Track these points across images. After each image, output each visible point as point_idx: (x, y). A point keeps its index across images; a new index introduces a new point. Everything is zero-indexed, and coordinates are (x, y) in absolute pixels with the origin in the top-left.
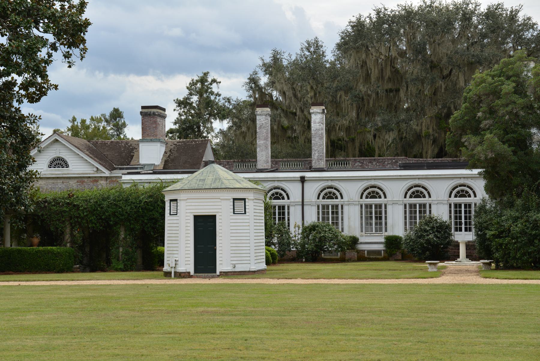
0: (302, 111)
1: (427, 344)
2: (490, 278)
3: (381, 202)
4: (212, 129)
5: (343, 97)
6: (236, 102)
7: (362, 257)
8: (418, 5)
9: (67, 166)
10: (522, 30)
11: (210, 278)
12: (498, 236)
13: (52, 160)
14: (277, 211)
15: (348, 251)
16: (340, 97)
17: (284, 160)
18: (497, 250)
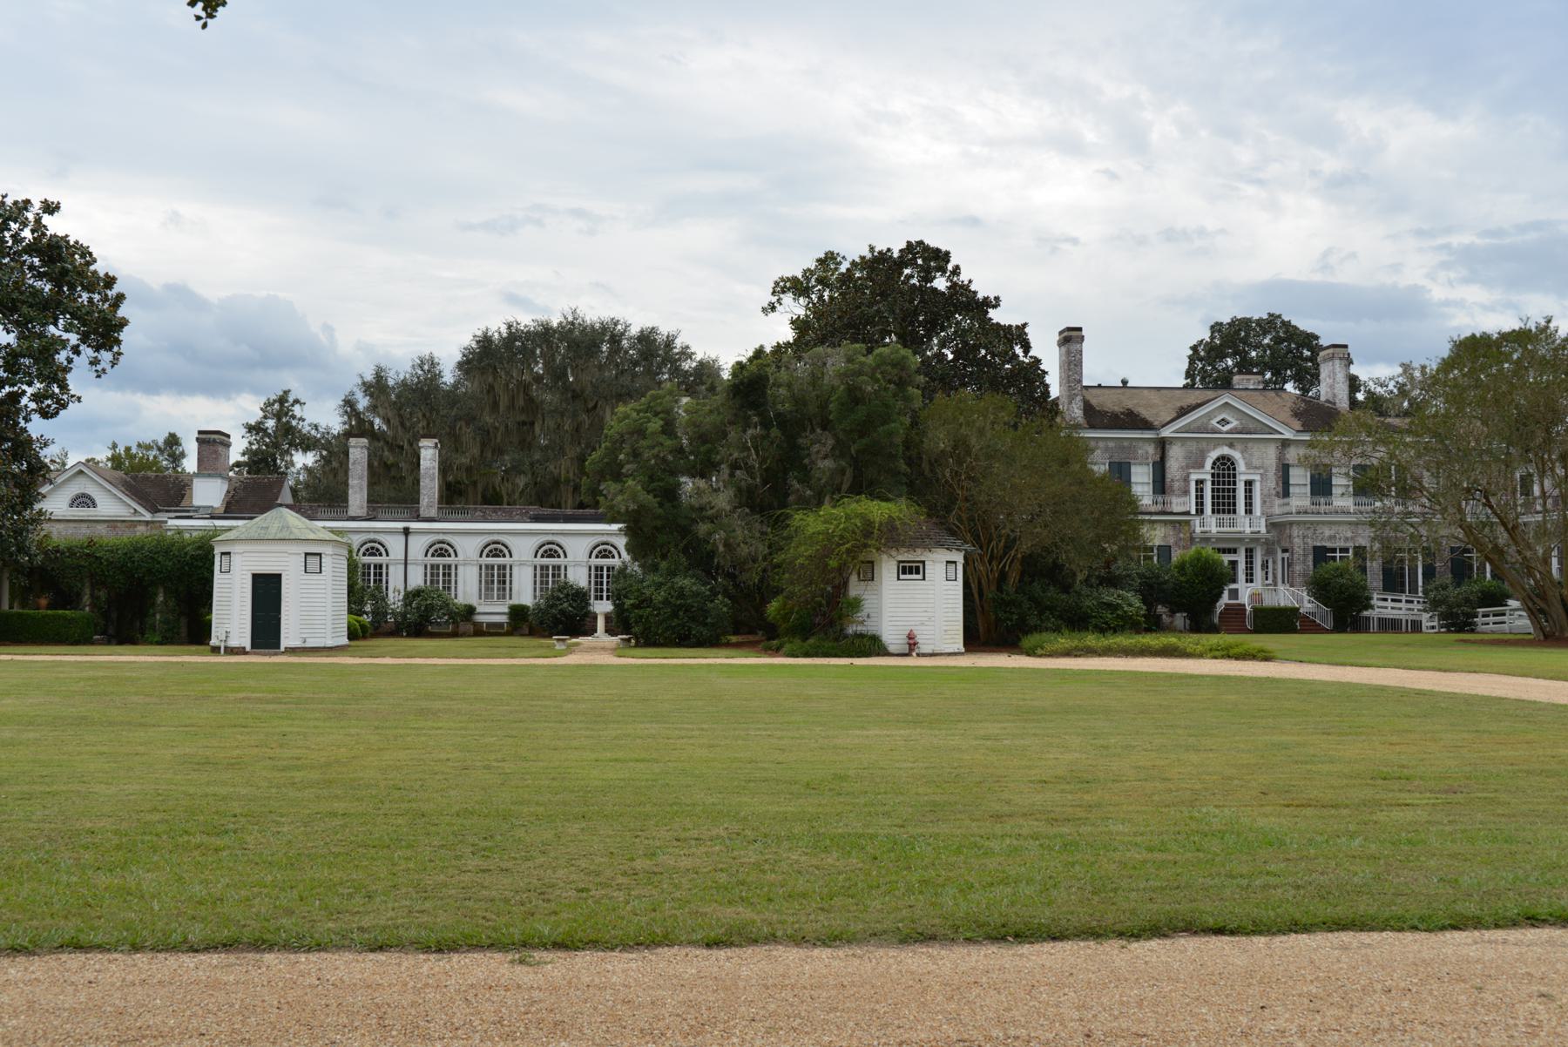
0: (411, 445)
1: (516, 740)
2: (624, 656)
4: (292, 464)
5: (464, 428)
7: (480, 631)
8: (558, 321)
9: (95, 505)
10: (679, 359)
11: (270, 655)
16: (460, 428)
18: (636, 622)
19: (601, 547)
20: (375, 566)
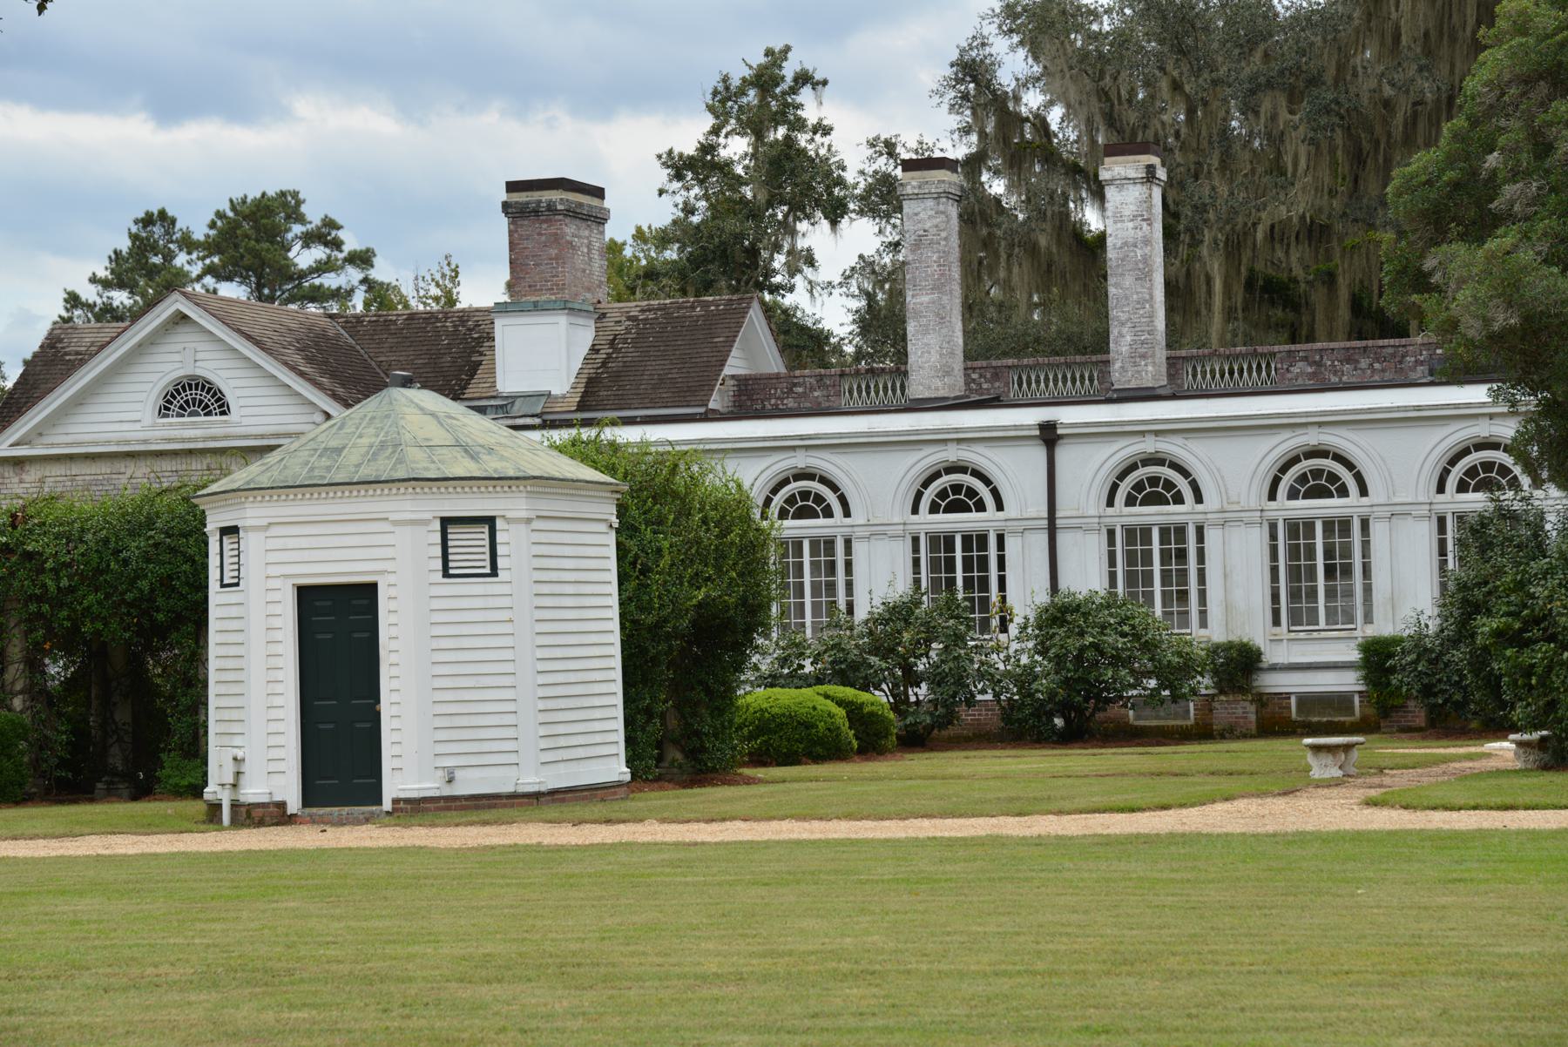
3: (1346, 512)
5: (1284, 115)
6: (916, 152)
12: (1518, 640)
13: (171, 388)
14: (959, 554)
15: (1223, 698)
17: (1025, 361)
19: (1475, 458)
20: (967, 539)
